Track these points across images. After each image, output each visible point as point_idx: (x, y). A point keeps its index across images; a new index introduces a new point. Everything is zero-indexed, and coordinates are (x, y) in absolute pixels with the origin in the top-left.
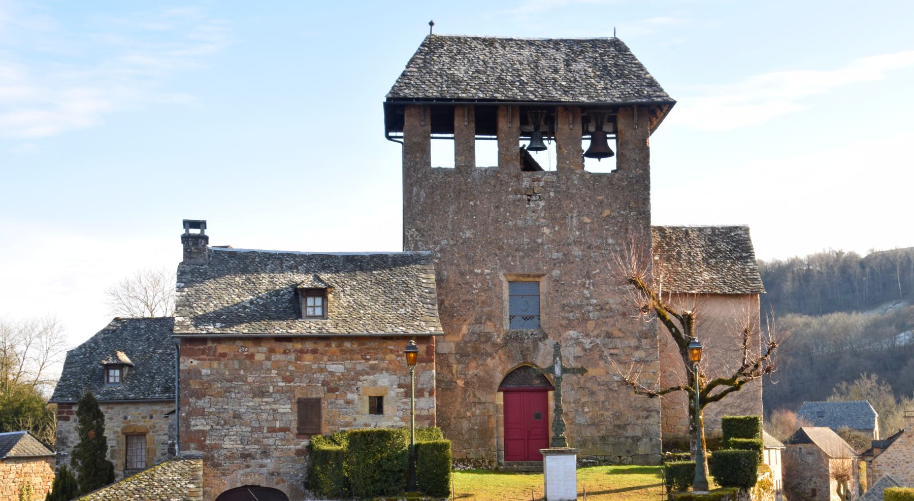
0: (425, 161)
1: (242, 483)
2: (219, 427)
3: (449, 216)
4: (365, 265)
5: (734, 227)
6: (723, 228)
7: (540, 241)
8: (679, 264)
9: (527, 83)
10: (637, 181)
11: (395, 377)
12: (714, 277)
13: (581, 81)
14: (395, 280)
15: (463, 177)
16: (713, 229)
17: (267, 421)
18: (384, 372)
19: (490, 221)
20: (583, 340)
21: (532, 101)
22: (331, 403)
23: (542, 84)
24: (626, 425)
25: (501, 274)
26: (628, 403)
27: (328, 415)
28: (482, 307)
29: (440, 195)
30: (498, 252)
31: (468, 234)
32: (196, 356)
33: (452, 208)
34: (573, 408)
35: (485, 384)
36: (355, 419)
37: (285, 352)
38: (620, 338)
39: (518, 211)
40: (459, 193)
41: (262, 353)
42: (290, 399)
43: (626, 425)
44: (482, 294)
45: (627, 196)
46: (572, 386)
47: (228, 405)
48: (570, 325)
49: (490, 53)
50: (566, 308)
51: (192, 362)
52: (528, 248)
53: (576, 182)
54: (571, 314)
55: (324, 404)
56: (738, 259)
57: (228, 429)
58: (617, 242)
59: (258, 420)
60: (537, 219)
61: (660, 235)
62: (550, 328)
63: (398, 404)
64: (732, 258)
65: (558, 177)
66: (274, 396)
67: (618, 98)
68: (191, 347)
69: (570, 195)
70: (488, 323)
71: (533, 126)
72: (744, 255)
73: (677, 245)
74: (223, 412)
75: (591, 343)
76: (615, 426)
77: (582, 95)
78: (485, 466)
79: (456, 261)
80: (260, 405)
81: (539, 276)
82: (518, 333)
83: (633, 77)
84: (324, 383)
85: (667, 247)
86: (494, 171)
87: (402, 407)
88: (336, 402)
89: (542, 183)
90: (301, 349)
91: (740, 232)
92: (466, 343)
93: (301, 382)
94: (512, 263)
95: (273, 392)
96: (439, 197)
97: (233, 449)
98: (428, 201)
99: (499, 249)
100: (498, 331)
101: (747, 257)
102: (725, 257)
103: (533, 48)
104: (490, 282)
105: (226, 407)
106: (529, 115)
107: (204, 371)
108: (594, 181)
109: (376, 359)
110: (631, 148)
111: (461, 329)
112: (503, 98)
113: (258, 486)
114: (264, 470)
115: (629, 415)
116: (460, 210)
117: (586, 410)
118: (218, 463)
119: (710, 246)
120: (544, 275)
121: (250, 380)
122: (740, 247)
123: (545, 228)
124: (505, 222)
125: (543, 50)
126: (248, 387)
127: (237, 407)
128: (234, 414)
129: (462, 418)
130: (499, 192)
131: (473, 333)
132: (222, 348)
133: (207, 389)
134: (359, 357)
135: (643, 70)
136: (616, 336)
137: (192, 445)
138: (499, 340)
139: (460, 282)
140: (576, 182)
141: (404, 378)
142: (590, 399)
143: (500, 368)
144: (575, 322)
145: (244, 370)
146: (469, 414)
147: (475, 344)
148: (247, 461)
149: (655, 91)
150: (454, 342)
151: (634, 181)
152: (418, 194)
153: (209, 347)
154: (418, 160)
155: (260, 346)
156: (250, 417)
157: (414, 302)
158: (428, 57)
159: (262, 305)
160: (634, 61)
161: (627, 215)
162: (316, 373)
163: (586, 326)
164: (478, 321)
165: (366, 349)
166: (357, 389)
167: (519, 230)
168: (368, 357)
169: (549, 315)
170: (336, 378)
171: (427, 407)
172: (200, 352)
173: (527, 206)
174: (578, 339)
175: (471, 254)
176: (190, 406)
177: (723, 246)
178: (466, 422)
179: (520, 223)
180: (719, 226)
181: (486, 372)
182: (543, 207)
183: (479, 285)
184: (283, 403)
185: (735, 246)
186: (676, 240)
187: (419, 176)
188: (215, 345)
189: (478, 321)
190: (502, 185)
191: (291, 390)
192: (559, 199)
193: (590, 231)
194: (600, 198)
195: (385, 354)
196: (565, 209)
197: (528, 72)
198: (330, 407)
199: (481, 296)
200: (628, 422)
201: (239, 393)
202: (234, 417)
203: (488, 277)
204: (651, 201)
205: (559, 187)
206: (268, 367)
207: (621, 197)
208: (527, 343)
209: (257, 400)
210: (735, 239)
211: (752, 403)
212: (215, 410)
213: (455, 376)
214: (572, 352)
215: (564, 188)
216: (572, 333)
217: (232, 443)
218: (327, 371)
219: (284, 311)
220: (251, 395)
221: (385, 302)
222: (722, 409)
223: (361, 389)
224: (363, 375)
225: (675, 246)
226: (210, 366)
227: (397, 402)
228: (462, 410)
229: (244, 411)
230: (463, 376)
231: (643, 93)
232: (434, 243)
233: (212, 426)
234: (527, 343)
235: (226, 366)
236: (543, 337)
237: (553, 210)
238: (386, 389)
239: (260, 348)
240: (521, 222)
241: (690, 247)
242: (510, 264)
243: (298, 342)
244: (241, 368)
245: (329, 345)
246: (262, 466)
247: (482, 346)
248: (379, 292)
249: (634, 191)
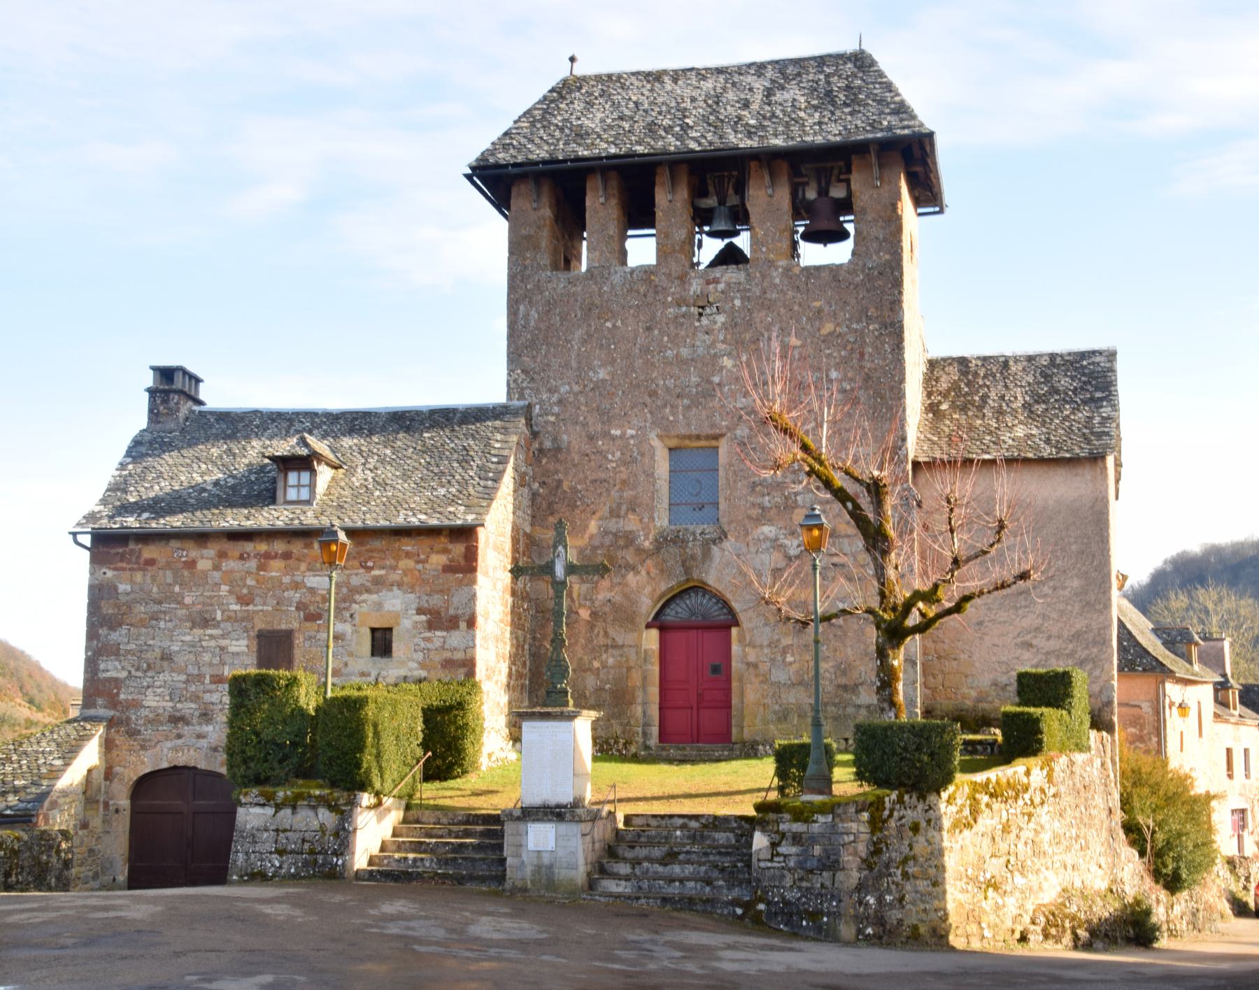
0: (538, 264)
1: (170, 762)
2: (139, 674)
3: (572, 346)
4: (417, 425)
5: (1089, 352)
6: (1069, 354)
7: (716, 379)
8: (980, 415)
9: (692, 128)
10: (881, 274)
11: (412, 596)
12: (1033, 432)
13: (781, 116)
14: (452, 445)
15: (596, 284)
16: (1053, 356)
17: (211, 665)
18: (395, 588)
19: (637, 351)
20: (786, 542)
21: (693, 151)
22: (310, 638)
23: (716, 127)
24: (856, 686)
25: (653, 435)
26: (862, 647)
27: (304, 656)
28: (621, 490)
29: (559, 314)
30: (648, 400)
31: (602, 374)
32: (111, 563)
33: (579, 333)
34: (766, 655)
35: (624, 615)
36: (346, 665)
37: (241, 557)
38: (849, 536)
39: (683, 333)
40: (590, 310)
41: (207, 558)
42: (246, 630)
43: (856, 686)
44: (622, 469)
45: (863, 299)
46: (767, 619)
47: (154, 639)
48: (764, 517)
49: (652, 90)
50: (758, 489)
51: (105, 573)
52: (697, 393)
53: (777, 281)
54: (767, 498)
55: (299, 640)
56: (1085, 402)
57: (153, 677)
58: (846, 376)
59: (197, 664)
60: (713, 344)
61: (959, 371)
62: (730, 523)
63: (416, 640)
64: (1076, 402)
65: (748, 275)
66: (222, 625)
67: (835, 135)
68: (105, 549)
69: (766, 302)
70: (631, 516)
71: (715, 198)
72: (1098, 395)
73: (985, 385)
74: (147, 651)
75: (799, 546)
76: (839, 686)
77: (776, 135)
78: (618, 751)
79: (582, 418)
80: (200, 641)
81: (717, 437)
82: (679, 531)
83: (870, 102)
84: (300, 606)
85: (966, 389)
86: (646, 272)
87: (423, 645)
88: (318, 637)
89: (721, 286)
90: (266, 552)
91: (1098, 359)
92: (594, 548)
93: (264, 604)
94: (671, 418)
95: (222, 620)
96: (558, 318)
97: (158, 708)
98: (542, 326)
99: (650, 396)
100: (646, 529)
101: (1102, 399)
102: (1064, 400)
103: (722, 78)
104: (635, 449)
105: (151, 642)
106: (709, 181)
107: (122, 587)
108: (808, 278)
109: (383, 568)
110: (870, 218)
111: (587, 527)
112: (646, 151)
113: (195, 768)
114: (203, 743)
115: (863, 669)
116: (590, 336)
117: (789, 659)
118: (135, 729)
119: (1042, 383)
120: (722, 435)
121: (188, 600)
122: (1094, 382)
123: (725, 358)
124: (661, 351)
125: (736, 78)
126: (184, 611)
127: (166, 644)
128: (163, 654)
129: (585, 671)
130: (651, 304)
131: (606, 533)
132: (149, 552)
133: (124, 614)
134: (356, 563)
135: (891, 91)
136: (843, 533)
137: (100, 701)
138: (647, 544)
139: (588, 451)
140: (777, 281)
141: (426, 598)
142: (795, 641)
143: (648, 590)
144: (773, 512)
145: (181, 585)
146: (596, 664)
147: (608, 551)
148: (178, 728)
149: (901, 120)
150: (576, 547)
151: (876, 273)
152: (527, 316)
153: (132, 550)
154: (528, 262)
155: (206, 548)
156: (185, 659)
157: (467, 477)
158: (553, 105)
159: (230, 488)
160: (879, 80)
161: (862, 331)
162: (288, 590)
163: (791, 519)
164: (615, 513)
165: (367, 551)
166: (352, 616)
167: (682, 362)
168: (370, 564)
169: (730, 500)
170: (318, 599)
171: (463, 646)
172: (118, 558)
173: (697, 324)
174: (776, 539)
175: (606, 405)
176: (99, 640)
177: (1064, 382)
178: (593, 677)
179: (685, 352)
180: (1064, 352)
181: (626, 596)
182: (723, 324)
183: (618, 454)
184: (236, 637)
185: (1085, 383)
186: (985, 377)
187: (529, 287)
188: (140, 546)
189: (615, 513)
190: (656, 293)
191: (248, 617)
192: (749, 310)
193: (799, 360)
194: (817, 304)
195: (397, 558)
196: (758, 325)
197: (701, 110)
198: (307, 644)
199: (620, 472)
200: (860, 681)
201: (170, 621)
202: (162, 659)
203: (632, 442)
204: (905, 306)
205: (749, 290)
206: (217, 580)
207: (853, 301)
208: (694, 548)
209: (198, 632)
210: (1086, 371)
211: (1095, 650)
212: (134, 646)
213: (577, 603)
214: (767, 562)
215: (757, 291)
216: (768, 530)
217: (157, 698)
218: (305, 587)
219: (259, 495)
220: (189, 624)
221: (421, 478)
222: (1041, 660)
223: (356, 616)
224: (360, 593)
225: (980, 386)
226: (131, 581)
227: (414, 636)
228: (585, 657)
229: (177, 649)
230: (588, 603)
231: (881, 124)
232: (549, 390)
233: (130, 672)
234: (694, 548)
235: (154, 579)
236: (720, 538)
237: (738, 328)
238: (397, 616)
239: (205, 552)
240: (686, 350)
241: (1006, 387)
242: (668, 419)
243: (262, 541)
244: (175, 583)
245: (309, 546)
246: (200, 736)
247: (620, 554)
248: (420, 464)
249: (875, 289)
